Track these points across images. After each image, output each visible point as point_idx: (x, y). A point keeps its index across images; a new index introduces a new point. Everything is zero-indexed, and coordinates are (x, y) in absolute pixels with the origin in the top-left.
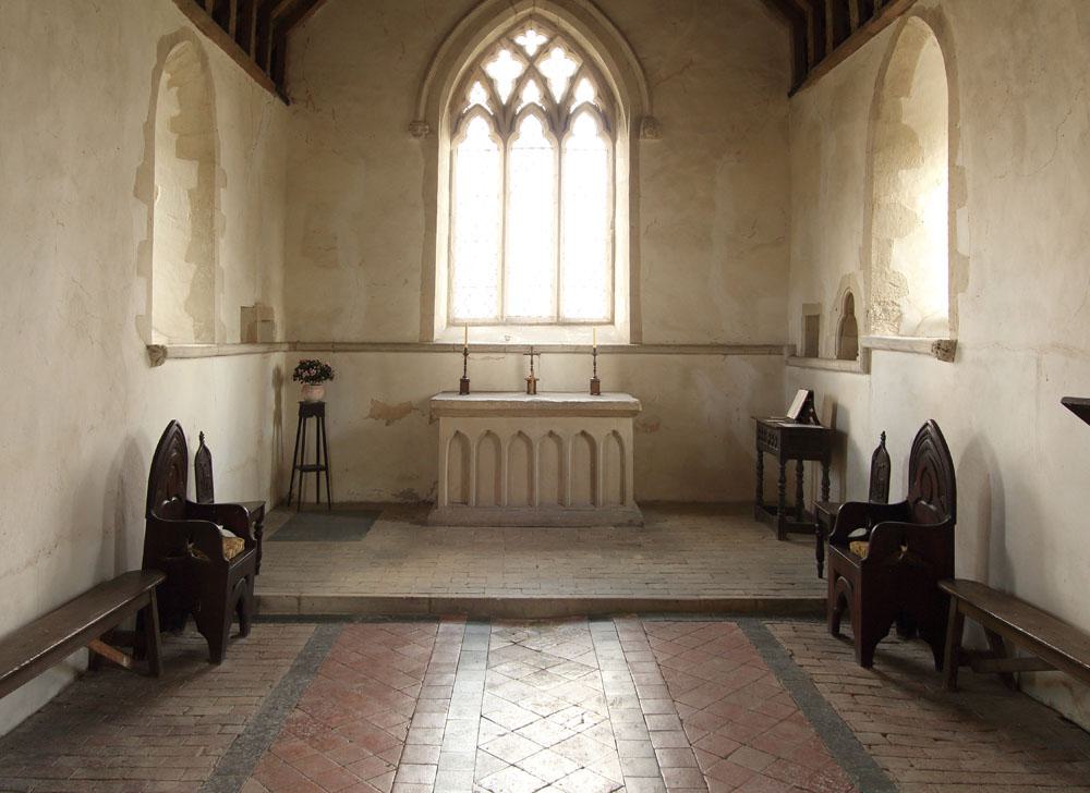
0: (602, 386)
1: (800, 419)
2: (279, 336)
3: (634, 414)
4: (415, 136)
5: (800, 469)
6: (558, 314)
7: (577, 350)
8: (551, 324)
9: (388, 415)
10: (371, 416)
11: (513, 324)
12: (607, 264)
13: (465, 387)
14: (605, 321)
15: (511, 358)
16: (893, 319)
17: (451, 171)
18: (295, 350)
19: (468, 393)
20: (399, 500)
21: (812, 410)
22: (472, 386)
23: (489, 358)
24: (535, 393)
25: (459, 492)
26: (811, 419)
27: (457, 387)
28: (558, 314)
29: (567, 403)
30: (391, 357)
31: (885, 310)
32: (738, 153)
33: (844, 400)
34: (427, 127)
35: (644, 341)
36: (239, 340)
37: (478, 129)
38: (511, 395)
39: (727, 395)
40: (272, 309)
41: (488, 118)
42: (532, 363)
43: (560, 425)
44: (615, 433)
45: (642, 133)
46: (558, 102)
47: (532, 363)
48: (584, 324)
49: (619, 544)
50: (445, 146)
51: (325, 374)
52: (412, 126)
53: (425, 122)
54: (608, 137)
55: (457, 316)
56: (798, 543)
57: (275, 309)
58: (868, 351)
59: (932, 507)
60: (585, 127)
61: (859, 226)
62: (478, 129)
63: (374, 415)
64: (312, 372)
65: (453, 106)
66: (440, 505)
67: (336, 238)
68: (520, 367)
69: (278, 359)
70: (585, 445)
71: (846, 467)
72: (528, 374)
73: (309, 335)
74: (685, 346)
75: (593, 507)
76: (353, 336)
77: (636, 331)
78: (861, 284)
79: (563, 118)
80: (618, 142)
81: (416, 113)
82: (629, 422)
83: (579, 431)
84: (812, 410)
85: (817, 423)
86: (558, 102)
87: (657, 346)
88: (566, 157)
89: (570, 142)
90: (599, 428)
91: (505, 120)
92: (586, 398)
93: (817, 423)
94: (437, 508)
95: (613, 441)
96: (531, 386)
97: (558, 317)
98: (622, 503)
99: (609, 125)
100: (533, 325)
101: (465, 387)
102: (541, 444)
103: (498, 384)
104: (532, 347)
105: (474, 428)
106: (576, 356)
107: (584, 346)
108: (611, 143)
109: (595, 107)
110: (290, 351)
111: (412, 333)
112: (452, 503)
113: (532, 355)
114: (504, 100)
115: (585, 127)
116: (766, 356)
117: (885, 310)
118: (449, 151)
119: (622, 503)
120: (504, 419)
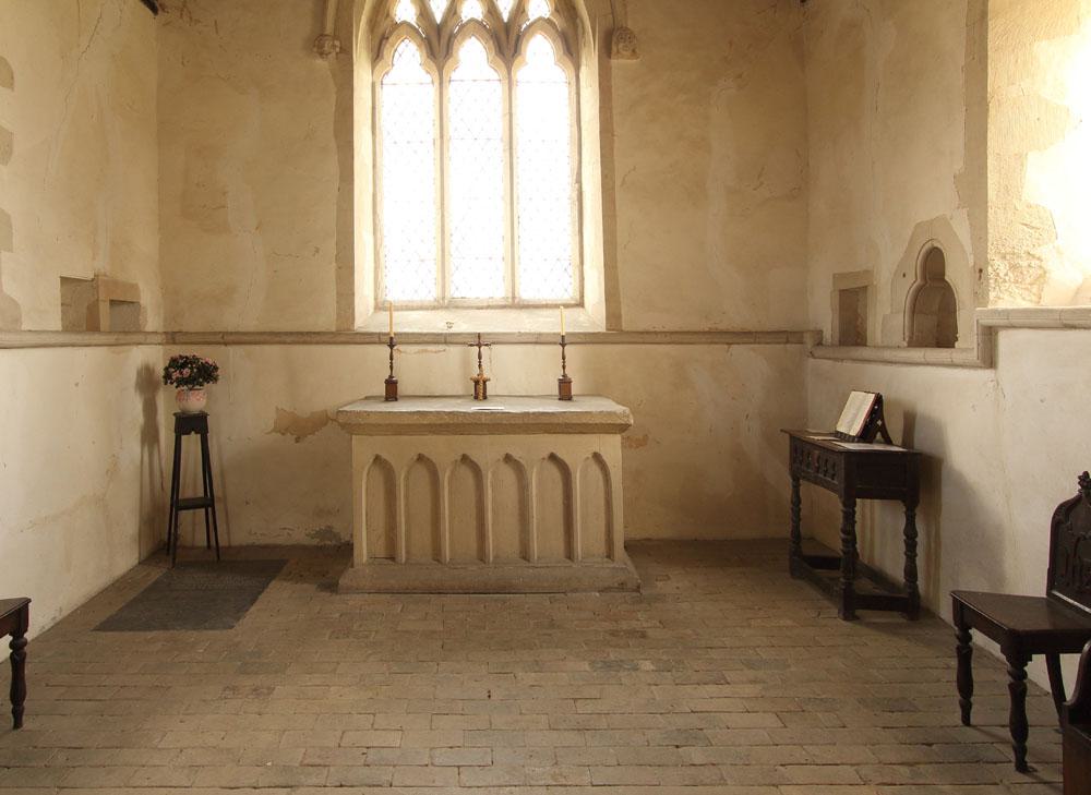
0: (575, 389)
1: (866, 434)
2: (153, 321)
3: (622, 428)
4: (321, 54)
5: (872, 506)
6: (513, 293)
7: (538, 340)
8: (504, 307)
9: (299, 428)
10: (274, 430)
11: (457, 307)
12: (572, 229)
13: (392, 391)
14: (573, 302)
15: (454, 352)
16: (1028, 280)
17: (374, 108)
18: (174, 343)
19: (396, 400)
20: (315, 542)
21: (879, 423)
22: (402, 389)
23: (426, 351)
24: (485, 398)
25: (382, 541)
26: (879, 436)
27: (381, 390)
28: (513, 293)
29: (528, 413)
30: (859, 365)
31: (1014, 267)
32: (740, 76)
33: (926, 406)
34: (337, 43)
35: (625, 327)
36: (57, 324)
37: (407, 56)
38: (453, 401)
39: (733, 398)
40: (137, 285)
41: (419, 40)
42: (480, 357)
43: (518, 445)
44: (597, 457)
45: (614, 49)
46: (506, 20)
47: (480, 357)
48: (546, 306)
49: (614, 633)
50: (362, 74)
51: (204, 374)
52: (317, 44)
53: (335, 37)
54: (570, 64)
55: (389, 298)
56: (868, 625)
57: (141, 286)
58: (989, 334)
59: (836, 482)
60: (540, 50)
61: (956, 140)
62: (407, 56)
63: (281, 429)
64: (193, 373)
65: (373, 24)
66: (356, 560)
67: (224, 194)
68: (466, 363)
69: (155, 356)
70: (554, 473)
71: (938, 510)
72: (475, 373)
73: (194, 323)
74: (695, 333)
75: (569, 563)
76: (250, 323)
77: (613, 315)
78: (962, 230)
79: (513, 37)
80: (583, 69)
81: (323, 26)
82: (617, 439)
83: (546, 454)
84: (879, 423)
85: (888, 441)
86: (506, 20)
87: (642, 333)
88: (518, 91)
89: (522, 73)
90: (575, 450)
91: (438, 42)
92: (555, 407)
93: (888, 441)
94: (352, 566)
95: (595, 470)
96: (479, 389)
97: (514, 298)
98: (608, 557)
99: (570, 47)
100: (482, 308)
101: (392, 391)
102: (494, 474)
103: (436, 382)
104: (479, 335)
105: (402, 452)
106: (538, 347)
107: (548, 334)
108: (573, 74)
109: (549, 21)
110: (168, 343)
111: (326, 321)
112: (373, 558)
113: (479, 345)
114: (438, 18)
115: (540, 50)
116: (782, 346)
117: (1014, 267)
118: (370, 81)
119: (608, 557)
120: (442, 438)
